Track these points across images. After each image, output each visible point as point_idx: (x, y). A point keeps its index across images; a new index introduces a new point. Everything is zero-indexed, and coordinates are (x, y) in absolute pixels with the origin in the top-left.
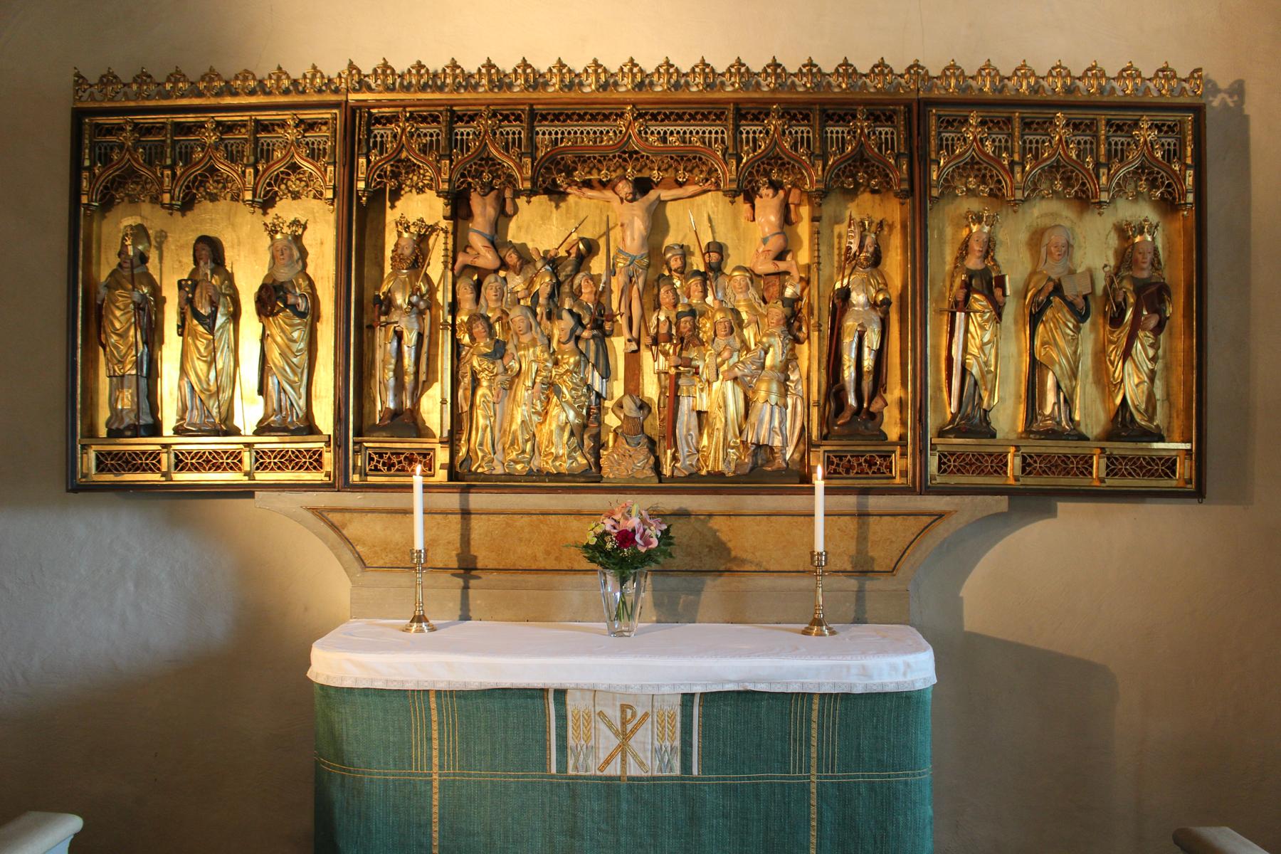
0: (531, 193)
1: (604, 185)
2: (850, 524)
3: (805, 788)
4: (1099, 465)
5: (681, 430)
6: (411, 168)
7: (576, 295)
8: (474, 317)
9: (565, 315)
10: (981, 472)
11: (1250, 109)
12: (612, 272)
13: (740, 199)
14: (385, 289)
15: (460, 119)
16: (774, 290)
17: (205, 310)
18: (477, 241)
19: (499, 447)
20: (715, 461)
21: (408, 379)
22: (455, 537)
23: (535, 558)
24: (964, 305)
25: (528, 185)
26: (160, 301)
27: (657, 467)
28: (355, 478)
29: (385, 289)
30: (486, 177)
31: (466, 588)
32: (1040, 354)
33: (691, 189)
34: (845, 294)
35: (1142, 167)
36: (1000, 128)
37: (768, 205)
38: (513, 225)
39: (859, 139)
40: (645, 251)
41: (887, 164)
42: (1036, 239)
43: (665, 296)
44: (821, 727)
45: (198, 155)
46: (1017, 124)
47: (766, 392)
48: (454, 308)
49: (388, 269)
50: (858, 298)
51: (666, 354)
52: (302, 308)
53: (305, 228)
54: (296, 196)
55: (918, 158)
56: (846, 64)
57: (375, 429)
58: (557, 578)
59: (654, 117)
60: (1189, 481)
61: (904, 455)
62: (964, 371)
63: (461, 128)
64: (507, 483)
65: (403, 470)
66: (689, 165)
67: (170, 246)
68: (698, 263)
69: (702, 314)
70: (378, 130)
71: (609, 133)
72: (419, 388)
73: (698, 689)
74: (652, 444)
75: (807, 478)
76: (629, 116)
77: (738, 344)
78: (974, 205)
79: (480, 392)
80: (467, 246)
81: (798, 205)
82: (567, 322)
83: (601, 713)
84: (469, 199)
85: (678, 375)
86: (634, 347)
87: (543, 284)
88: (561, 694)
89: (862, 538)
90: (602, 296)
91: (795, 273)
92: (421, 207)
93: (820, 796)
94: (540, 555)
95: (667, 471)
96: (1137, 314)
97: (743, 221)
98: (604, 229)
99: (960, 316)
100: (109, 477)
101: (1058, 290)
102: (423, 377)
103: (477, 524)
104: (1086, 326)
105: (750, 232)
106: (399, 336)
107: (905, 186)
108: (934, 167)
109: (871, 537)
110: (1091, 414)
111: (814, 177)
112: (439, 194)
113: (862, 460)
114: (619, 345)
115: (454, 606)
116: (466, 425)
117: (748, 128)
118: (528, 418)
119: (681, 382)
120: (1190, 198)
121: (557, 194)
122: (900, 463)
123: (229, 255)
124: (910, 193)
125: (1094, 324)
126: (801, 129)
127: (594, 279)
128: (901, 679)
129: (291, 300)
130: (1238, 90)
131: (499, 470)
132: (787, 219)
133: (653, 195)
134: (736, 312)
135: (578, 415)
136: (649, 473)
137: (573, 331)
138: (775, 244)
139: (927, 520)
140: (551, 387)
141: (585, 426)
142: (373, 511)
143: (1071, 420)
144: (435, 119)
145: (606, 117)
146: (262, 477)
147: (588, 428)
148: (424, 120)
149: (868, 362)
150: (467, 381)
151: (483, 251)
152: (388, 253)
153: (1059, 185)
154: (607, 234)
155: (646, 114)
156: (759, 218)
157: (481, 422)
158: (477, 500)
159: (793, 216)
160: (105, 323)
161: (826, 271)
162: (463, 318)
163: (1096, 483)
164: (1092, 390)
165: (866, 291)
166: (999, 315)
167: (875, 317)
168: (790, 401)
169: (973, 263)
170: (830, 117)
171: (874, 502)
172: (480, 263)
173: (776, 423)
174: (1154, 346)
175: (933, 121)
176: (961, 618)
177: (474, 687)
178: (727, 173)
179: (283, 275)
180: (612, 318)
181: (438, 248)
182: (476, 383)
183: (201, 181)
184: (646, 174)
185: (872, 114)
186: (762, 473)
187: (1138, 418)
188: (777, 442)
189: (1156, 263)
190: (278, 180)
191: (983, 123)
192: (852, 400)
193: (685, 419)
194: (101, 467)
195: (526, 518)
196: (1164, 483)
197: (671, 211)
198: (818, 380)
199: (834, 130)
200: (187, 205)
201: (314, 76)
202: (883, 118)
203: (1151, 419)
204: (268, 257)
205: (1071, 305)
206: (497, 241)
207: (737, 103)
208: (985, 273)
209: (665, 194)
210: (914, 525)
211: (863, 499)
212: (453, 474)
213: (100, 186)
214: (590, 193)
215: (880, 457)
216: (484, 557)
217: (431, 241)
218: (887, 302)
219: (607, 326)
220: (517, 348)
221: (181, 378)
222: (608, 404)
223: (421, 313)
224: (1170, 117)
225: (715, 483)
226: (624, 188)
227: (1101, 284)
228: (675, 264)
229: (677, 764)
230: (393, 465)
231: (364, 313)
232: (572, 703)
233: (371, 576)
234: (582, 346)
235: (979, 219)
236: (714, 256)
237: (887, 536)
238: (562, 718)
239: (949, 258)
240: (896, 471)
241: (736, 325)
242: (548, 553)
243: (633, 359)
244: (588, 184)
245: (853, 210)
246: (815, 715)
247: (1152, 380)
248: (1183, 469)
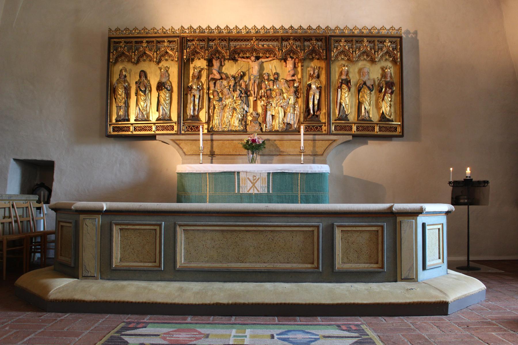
0: (229, 59)
1: (247, 58)
2: (311, 143)
3: (297, 196)
4: (377, 129)
5: (268, 119)
6: (198, 53)
7: (240, 86)
8: (214, 91)
9: (238, 90)
11: (419, 38)
12: (250, 80)
13: (283, 61)
14: (190, 84)
15: (211, 40)
16: (292, 84)
17: (143, 89)
18: (215, 72)
19: (220, 124)
20: (277, 128)
21: (197, 108)
22: (209, 146)
23: (230, 152)
24: (340, 87)
25: (228, 57)
26: (130, 88)
27: (261, 129)
28: (183, 132)
29: (190, 84)
30: (217, 55)
31: (212, 159)
32: (361, 100)
33: (270, 59)
34: (310, 86)
35: (387, 52)
37: (290, 64)
38: (224, 68)
39: (314, 46)
40: (258, 74)
41: (320, 52)
42: (360, 71)
43: (263, 86)
44: (301, 181)
45: (141, 49)
46: (354, 42)
47: (290, 110)
48: (209, 89)
49: (191, 79)
50: (313, 86)
51: (264, 100)
52: (169, 89)
53: (169, 68)
54: (167, 60)
55: (328, 50)
56: (310, 26)
57: (188, 120)
58: (236, 157)
59: (261, 40)
61: (325, 126)
63: (211, 43)
64: (223, 133)
66: (269, 52)
67: (133, 73)
68: (272, 78)
69: (273, 90)
70: (189, 43)
71: (249, 44)
72: (200, 109)
73: (271, 172)
74: (260, 124)
75: (299, 132)
76: (254, 40)
77: (282, 98)
78: (343, 62)
79: (215, 110)
80: (212, 73)
81: (298, 63)
82: (238, 92)
83: (248, 178)
84: (212, 61)
85: (267, 105)
86: (255, 99)
87: (232, 83)
88: (238, 173)
89: (314, 146)
90: (247, 86)
91: (297, 80)
92: (200, 63)
93: (301, 198)
94: (231, 151)
95: (264, 130)
96: (386, 89)
97: (284, 67)
98: (248, 69)
99: (339, 90)
100: (116, 133)
101: (365, 83)
102: (200, 107)
103: (215, 143)
104: (373, 92)
105: (285, 70)
106: (194, 96)
107: (325, 57)
109: (317, 146)
110: (375, 117)
111: (302, 55)
112: (205, 59)
114: (252, 99)
115: (210, 160)
116: (211, 119)
117: (284, 43)
118: (228, 118)
119: (268, 107)
120: (399, 60)
121: (235, 60)
122: (324, 128)
123: (149, 75)
124: (326, 59)
125: (375, 93)
126: (298, 43)
127: (246, 82)
128: (320, 170)
129: (166, 86)
130: (416, 33)
131: (220, 130)
132: (295, 67)
133: (260, 60)
134: (282, 90)
135: (241, 116)
136: (259, 130)
137: (240, 94)
138: (292, 73)
139: (331, 142)
140: (234, 109)
141: (242, 119)
142: (188, 140)
143: (369, 117)
144: (204, 40)
145: (248, 40)
146: (157, 132)
147: (243, 120)
148: (201, 41)
149: (316, 102)
150: (212, 108)
151: (216, 74)
152: (191, 75)
153: (365, 57)
154: (249, 70)
156: (288, 66)
157: (216, 118)
158: (215, 137)
159: (296, 66)
160: (116, 92)
161: (305, 80)
162: (211, 91)
163: (376, 133)
164: (375, 110)
165: (315, 85)
167: (318, 91)
168: (296, 112)
169: (344, 77)
170: (306, 40)
171: (317, 137)
172: (216, 77)
173: (292, 118)
174: (391, 97)
175: (332, 41)
176: (343, 171)
177: (218, 172)
178: (279, 54)
179: (164, 80)
180: (249, 91)
181: (204, 74)
182: (214, 108)
183: (142, 56)
184: (258, 55)
186: (288, 130)
187: (386, 116)
188: (292, 122)
189: (391, 77)
190: (163, 56)
191: (345, 41)
192: (312, 112)
193: (269, 118)
194: (114, 131)
195: (228, 142)
196: (394, 133)
197: (265, 65)
198: (303, 107)
199: (307, 43)
200: (138, 62)
201: (172, 29)
203: (390, 117)
204: (159, 77)
205: (369, 88)
206: (220, 73)
207: (282, 36)
208: (346, 80)
209: (263, 60)
210: (328, 143)
211: (314, 136)
212: (208, 131)
213: (115, 57)
214: (244, 60)
216: (216, 151)
217: (202, 72)
218: (320, 87)
219: (249, 93)
220: (225, 99)
221: (136, 106)
222: (248, 114)
223: (200, 90)
224: (394, 40)
225: (277, 132)
226: (253, 58)
227: (377, 83)
228: (266, 78)
229: (266, 190)
231: (185, 91)
232: (242, 175)
233: (187, 157)
234: (242, 99)
235: (344, 66)
236: (276, 76)
237: (320, 146)
238: (239, 179)
239: (337, 77)
240: (323, 129)
241: (281, 93)
242: (233, 150)
243: (255, 102)
244: (243, 58)
245: (312, 64)
246: (299, 178)
247: (390, 107)
248: (399, 130)
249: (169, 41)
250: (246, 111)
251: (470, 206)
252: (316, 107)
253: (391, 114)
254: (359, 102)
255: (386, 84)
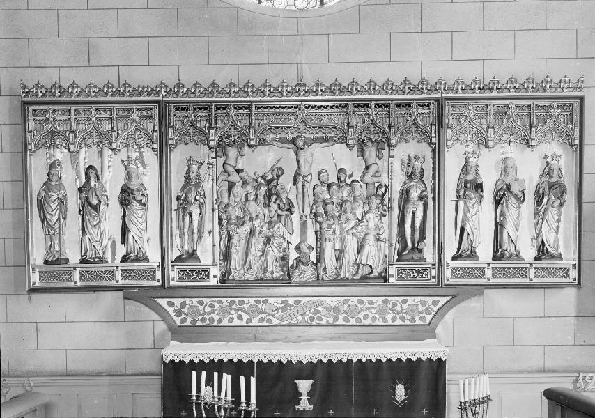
46: (73, 111)
60: (575, 279)
101: (508, 188)
149: (418, 223)
192: (409, 244)
203: (557, 249)
205: (516, 196)
248: (573, 274)
251: (20, 126)
253: (558, 245)
254: (496, 224)
255: (550, 189)
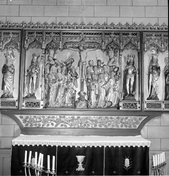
4: (163, 106)
10: (156, 107)
36: (159, 37)
46: (162, 35)
62: (152, 86)
65: (33, 106)
99: (151, 75)
108: (145, 44)
113: (130, 105)
149: (132, 83)
155: (166, 35)
166: (159, 75)
167: (133, 75)
185: (132, 34)
192: (128, 92)
202: (135, 34)
215: (134, 104)
230: (31, 105)
249: (13, 33)
250: (75, 91)
252: (132, 89)
